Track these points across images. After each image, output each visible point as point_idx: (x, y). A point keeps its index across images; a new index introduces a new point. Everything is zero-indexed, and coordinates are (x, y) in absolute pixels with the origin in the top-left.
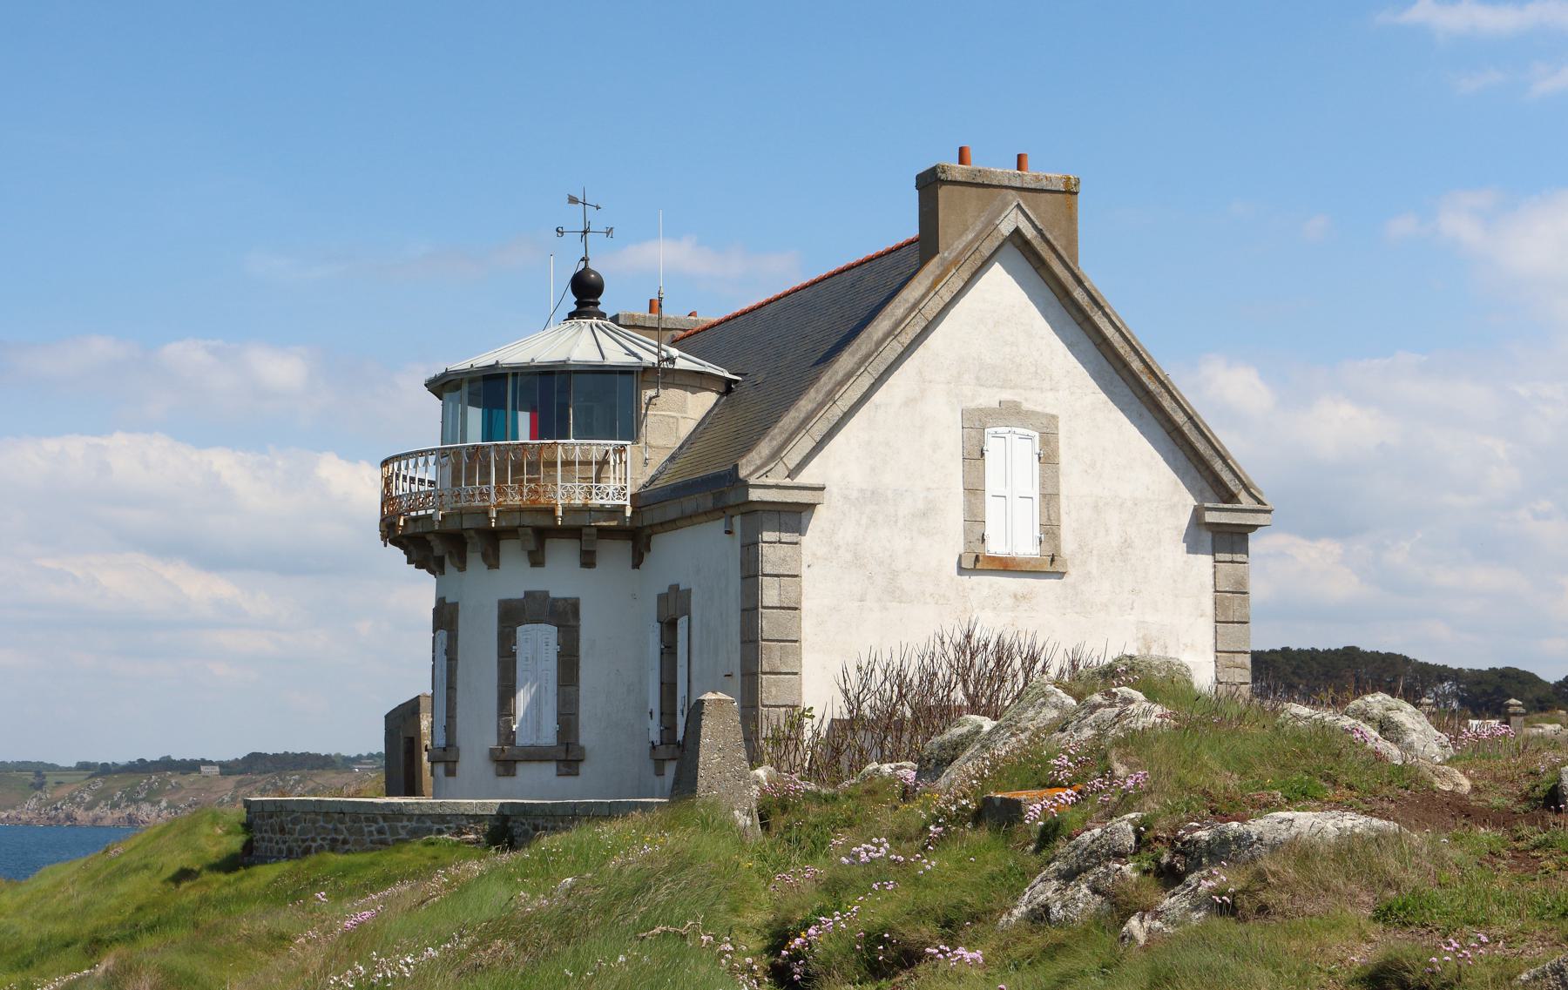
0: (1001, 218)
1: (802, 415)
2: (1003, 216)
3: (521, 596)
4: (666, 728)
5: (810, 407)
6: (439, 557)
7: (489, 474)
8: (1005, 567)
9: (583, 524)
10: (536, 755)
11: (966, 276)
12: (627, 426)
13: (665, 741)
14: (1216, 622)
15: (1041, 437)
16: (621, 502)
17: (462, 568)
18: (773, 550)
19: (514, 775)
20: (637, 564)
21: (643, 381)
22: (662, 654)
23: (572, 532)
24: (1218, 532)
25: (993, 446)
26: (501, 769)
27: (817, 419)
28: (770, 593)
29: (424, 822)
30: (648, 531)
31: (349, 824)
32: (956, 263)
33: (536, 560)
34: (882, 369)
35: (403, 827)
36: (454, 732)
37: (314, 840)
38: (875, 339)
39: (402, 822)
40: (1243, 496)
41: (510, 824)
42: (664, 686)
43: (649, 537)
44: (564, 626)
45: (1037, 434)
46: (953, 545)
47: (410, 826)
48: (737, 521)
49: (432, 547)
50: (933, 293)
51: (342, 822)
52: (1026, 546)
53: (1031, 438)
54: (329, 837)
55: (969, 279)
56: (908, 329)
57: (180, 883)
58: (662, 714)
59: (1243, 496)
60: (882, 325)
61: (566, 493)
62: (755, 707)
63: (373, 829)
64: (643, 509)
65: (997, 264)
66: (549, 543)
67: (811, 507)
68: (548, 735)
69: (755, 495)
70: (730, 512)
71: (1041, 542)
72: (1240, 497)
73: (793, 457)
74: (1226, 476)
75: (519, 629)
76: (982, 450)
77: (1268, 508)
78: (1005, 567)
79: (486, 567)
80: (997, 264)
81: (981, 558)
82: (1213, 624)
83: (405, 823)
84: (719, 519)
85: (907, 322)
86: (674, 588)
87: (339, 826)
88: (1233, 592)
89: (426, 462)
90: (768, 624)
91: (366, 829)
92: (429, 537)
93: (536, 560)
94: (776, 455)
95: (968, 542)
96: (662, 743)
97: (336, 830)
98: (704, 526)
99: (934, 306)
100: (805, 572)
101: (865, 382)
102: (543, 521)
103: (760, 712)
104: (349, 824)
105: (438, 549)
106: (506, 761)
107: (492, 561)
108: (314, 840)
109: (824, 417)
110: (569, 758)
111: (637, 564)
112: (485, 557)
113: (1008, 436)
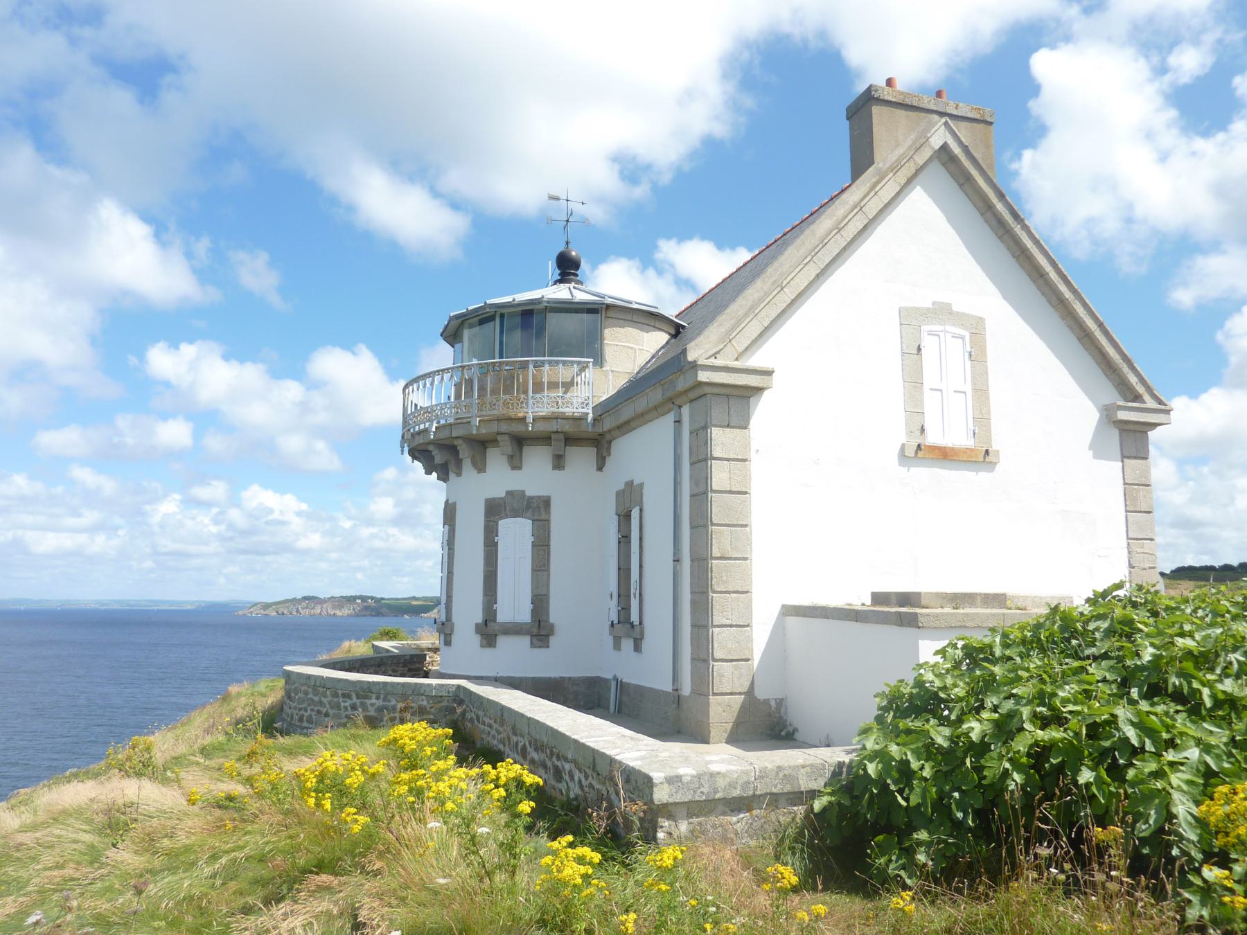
0: (932, 132)
1: (749, 304)
2: (933, 130)
3: (503, 495)
4: (623, 609)
5: (756, 295)
6: (442, 465)
7: (472, 390)
8: (945, 456)
9: (552, 430)
10: (514, 629)
11: (903, 181)
12: (592, 349)
13: (621, 620)
14: (1127, 511)
15: (971, 337)
16: (584, 410)
17: (459, 475)
18: (721, 439)
19: (495, 647)
20: (600, 468)
21: (606, 317)
22: (619, 542)
23: (544, 439)
24: (1124, 430)
25: (929, 344)
26: (484, 642)
27: (765, 303)
28: (720, 476)
29: (389, 701)
30: (608, 437)
31: (330, 698)
32: (895, 168)
33: (515, 463)
34: (827, 260)
35: (372, 705)
36: (451, 610)
37: (306, 710)
38: (818, 236)
39: (370, 699)
40: (1147, 397)
41: (352, 774)
42: (621, 571)
43: (610, 442)
44: (537, 520)
45: (967, 334)
46: (898, 436)
47: (378, 704)
48: (686, 410)
49: (433, 457)
50: (873, 193)
51: (325, 696)
52: (958, 436)
53: (962, 338)
54: (316, 709)
55: (905, 184)
56: (851, 225)
57: (1100, 411)
58: (619, 596)
59: (1147, 397)
60: (825, 223)
61: (536, 408)
62: (705, 593)
63: (347, 704)
64: (602, 417)
65: (918, 187)
66: (526, 450)
67: (759, 390)
68: (524, 614)
69: (703, 376)
70: (678, 402)
71: (974, 434)
72: (1144, 398)
73: (741, 343)
74: (1133, 379)
75: (501, 523)
76: (919, 346)
77: (1167, 408)
78: (945, 456)
79: (476, 471)
80: (918, 187)
81: (923, 447)
82: (1124, 514)
83: (374, 701)
84: (668, 413)
85: (849, 217)
86: (630, 484)
87: (323, 699)
88: (1138, 485)
89: (425, 386)
90: (719, 508)
91: (342, 704)
92: (431, 448)
93: (515, 463)
94: (728, 339)
95: (910, 433)
96: (619, 622)
97: (321, 703)
98: (656, 422)
99: (872, 207)
100: (753, 456)
101: (812, 271)
102: (516, 428)
103: (710, 597)
104: (330, 698)
105: (439, 458)
106: (489, 632)
107: (480, 467)
108: (306, 710)
109: (772, 302)
110: (542, 633)
111: (600, 468)
112: (474, 464)
113: (942, 334)
